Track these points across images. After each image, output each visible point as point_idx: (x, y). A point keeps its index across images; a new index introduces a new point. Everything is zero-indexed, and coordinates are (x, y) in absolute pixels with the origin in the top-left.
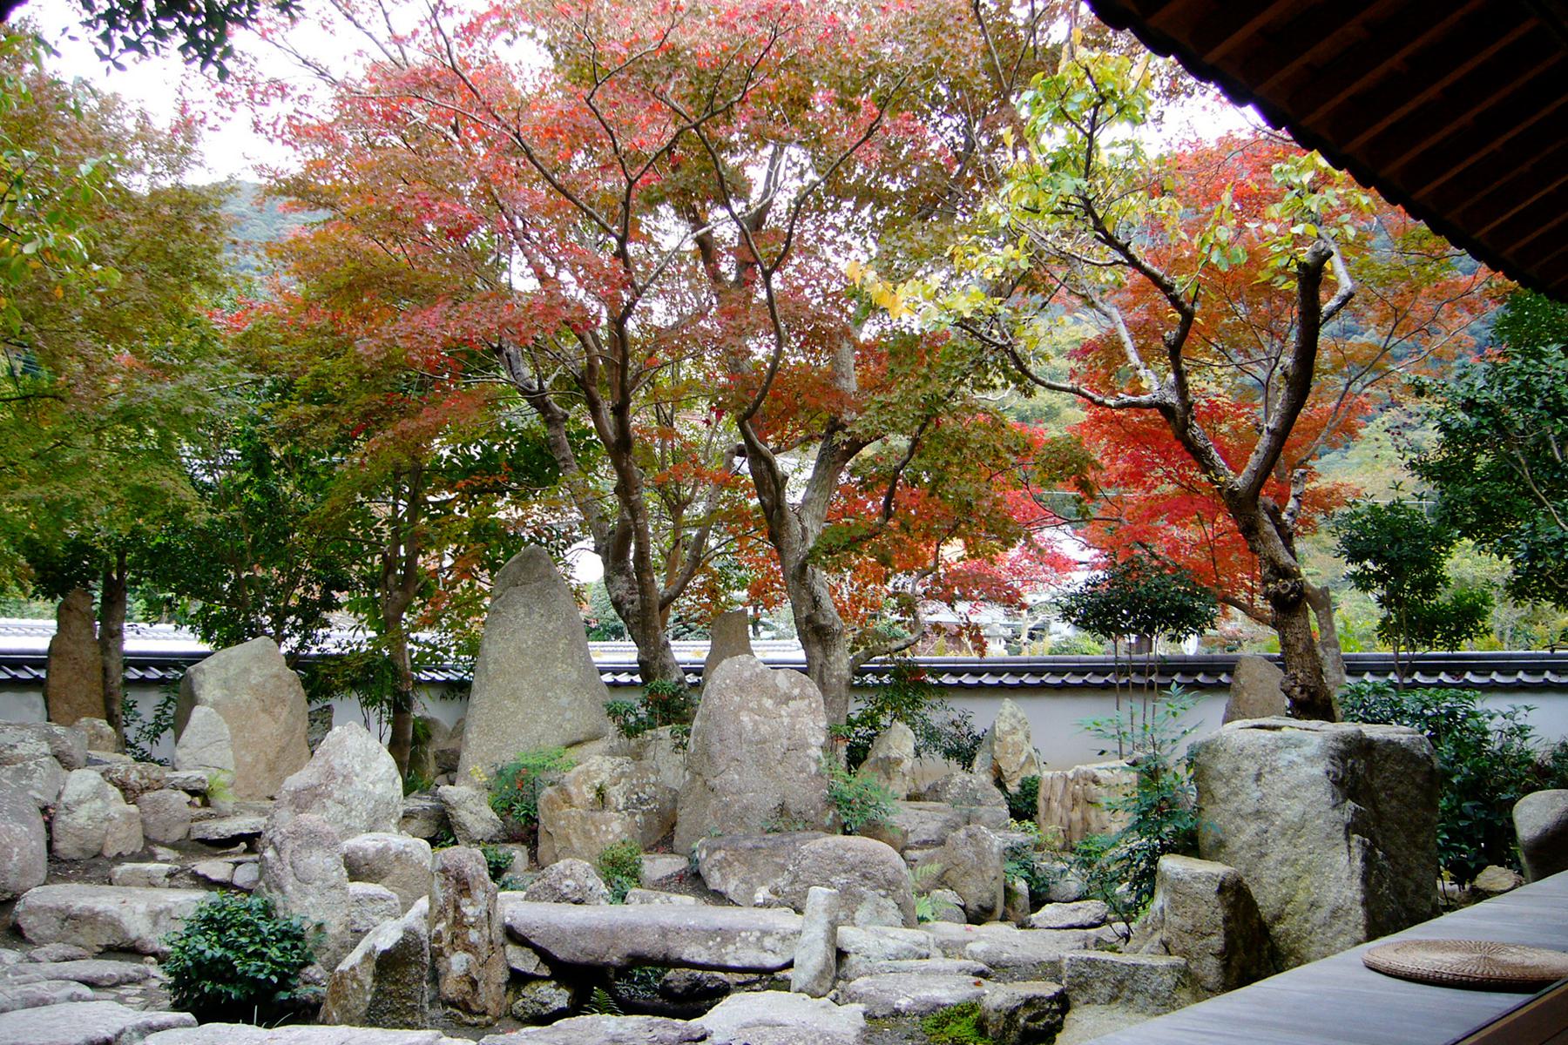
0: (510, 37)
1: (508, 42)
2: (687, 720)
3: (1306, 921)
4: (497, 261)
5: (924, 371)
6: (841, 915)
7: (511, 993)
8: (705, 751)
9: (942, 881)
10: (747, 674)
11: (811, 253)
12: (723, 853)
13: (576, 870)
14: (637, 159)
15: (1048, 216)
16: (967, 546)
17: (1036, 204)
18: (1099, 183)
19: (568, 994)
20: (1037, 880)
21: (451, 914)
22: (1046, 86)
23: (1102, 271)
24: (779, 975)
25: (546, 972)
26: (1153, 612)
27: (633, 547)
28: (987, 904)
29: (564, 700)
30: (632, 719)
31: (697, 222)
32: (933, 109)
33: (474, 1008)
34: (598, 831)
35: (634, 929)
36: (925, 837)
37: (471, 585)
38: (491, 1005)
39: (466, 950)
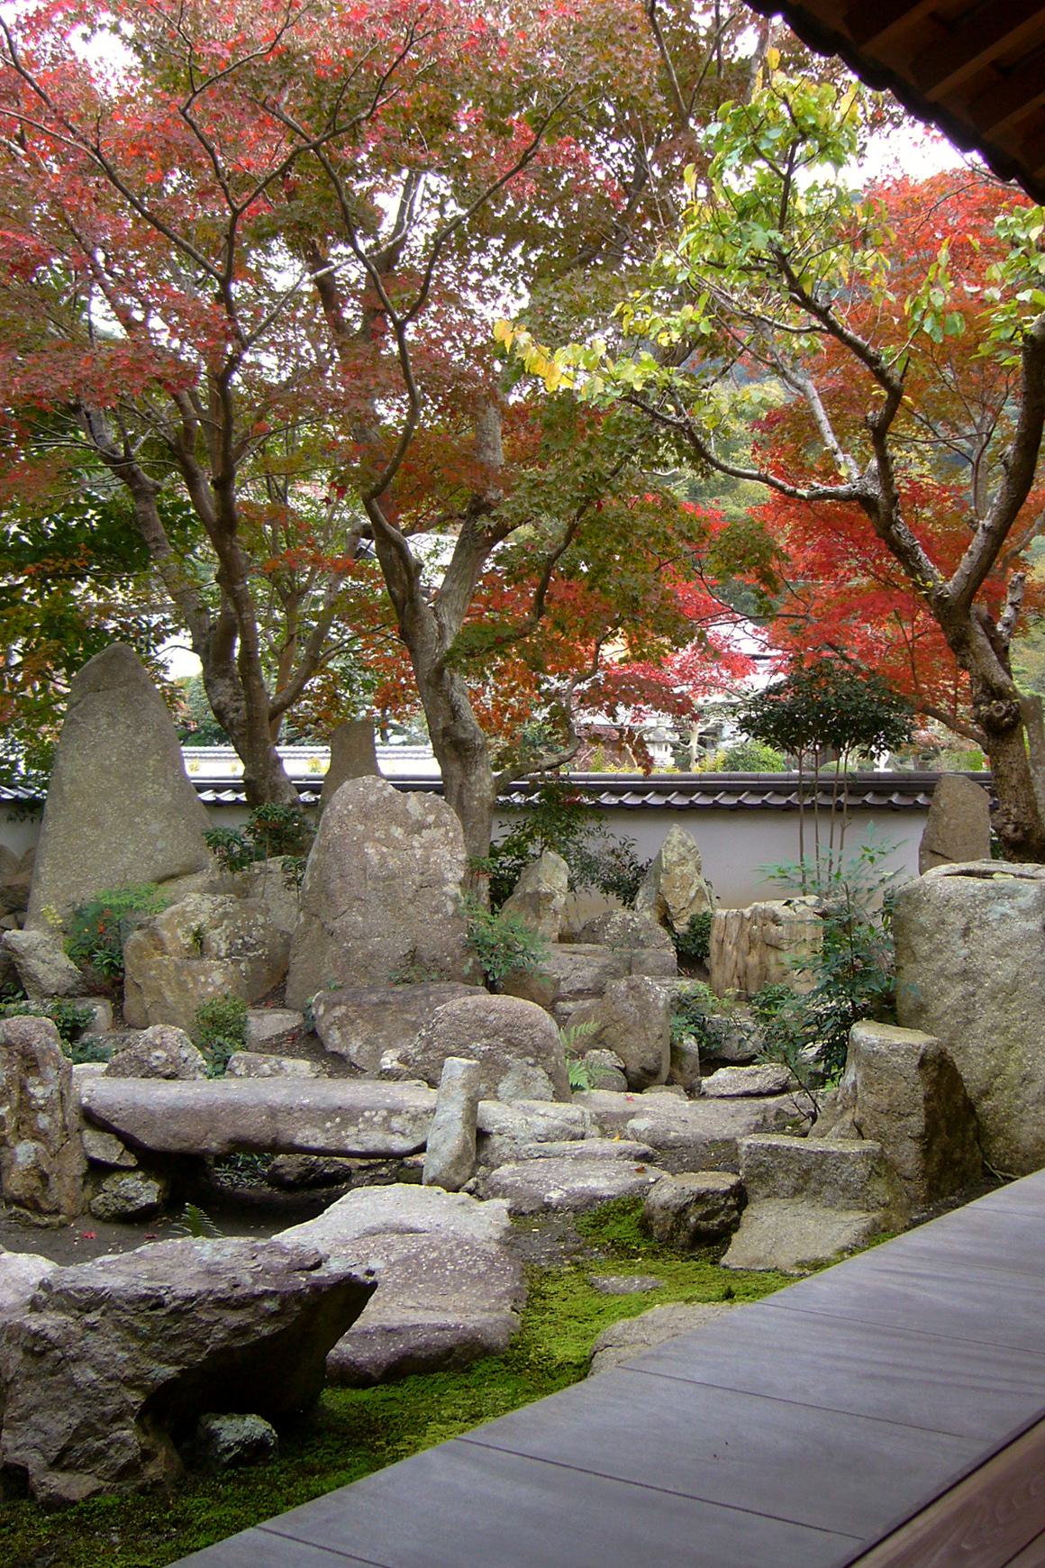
0: (88, 31)
1: (85, 38)
2: (302, 850)
3: (1017, 1096)
4: (74, 300)
5: (585, 445)
6: (483, 1087)
7: (89, 1187)
8: (323, 888)
9: (598, 1040)
10: (373, 798)
11: (452, 298)
12: (343, 1009)
13: (167, 1038)
14: (245, 182)
15: (735, 273)
16: (631, 646)
17: (722, 258)
18: (795, 234)
19: (157, 1186)
20: (708, 1036)
21: (15, 1094)
22: (736, 118)
23: (795, 332)
24: (409, 1161)
25: (132, 1162)
26: (843, 724)
27: (238, 642)
28: (651, 1066)
29: (156, 827)
30: (237, 849)
31: (315, 260)
32: (598, 130)
33: (45, 1206)
34: (196, 982)
35: (236, 1109)
36: (579, 986)
37: (44, 687)
38: (65, 1201)
39: (34, 1138)
